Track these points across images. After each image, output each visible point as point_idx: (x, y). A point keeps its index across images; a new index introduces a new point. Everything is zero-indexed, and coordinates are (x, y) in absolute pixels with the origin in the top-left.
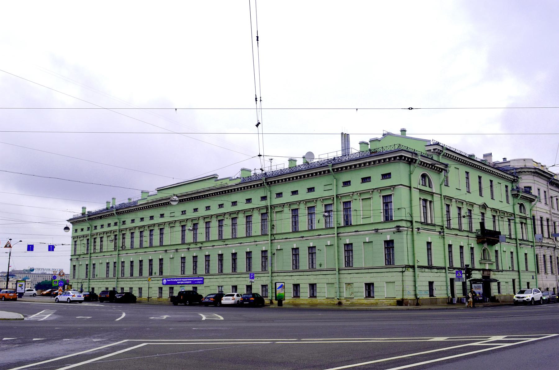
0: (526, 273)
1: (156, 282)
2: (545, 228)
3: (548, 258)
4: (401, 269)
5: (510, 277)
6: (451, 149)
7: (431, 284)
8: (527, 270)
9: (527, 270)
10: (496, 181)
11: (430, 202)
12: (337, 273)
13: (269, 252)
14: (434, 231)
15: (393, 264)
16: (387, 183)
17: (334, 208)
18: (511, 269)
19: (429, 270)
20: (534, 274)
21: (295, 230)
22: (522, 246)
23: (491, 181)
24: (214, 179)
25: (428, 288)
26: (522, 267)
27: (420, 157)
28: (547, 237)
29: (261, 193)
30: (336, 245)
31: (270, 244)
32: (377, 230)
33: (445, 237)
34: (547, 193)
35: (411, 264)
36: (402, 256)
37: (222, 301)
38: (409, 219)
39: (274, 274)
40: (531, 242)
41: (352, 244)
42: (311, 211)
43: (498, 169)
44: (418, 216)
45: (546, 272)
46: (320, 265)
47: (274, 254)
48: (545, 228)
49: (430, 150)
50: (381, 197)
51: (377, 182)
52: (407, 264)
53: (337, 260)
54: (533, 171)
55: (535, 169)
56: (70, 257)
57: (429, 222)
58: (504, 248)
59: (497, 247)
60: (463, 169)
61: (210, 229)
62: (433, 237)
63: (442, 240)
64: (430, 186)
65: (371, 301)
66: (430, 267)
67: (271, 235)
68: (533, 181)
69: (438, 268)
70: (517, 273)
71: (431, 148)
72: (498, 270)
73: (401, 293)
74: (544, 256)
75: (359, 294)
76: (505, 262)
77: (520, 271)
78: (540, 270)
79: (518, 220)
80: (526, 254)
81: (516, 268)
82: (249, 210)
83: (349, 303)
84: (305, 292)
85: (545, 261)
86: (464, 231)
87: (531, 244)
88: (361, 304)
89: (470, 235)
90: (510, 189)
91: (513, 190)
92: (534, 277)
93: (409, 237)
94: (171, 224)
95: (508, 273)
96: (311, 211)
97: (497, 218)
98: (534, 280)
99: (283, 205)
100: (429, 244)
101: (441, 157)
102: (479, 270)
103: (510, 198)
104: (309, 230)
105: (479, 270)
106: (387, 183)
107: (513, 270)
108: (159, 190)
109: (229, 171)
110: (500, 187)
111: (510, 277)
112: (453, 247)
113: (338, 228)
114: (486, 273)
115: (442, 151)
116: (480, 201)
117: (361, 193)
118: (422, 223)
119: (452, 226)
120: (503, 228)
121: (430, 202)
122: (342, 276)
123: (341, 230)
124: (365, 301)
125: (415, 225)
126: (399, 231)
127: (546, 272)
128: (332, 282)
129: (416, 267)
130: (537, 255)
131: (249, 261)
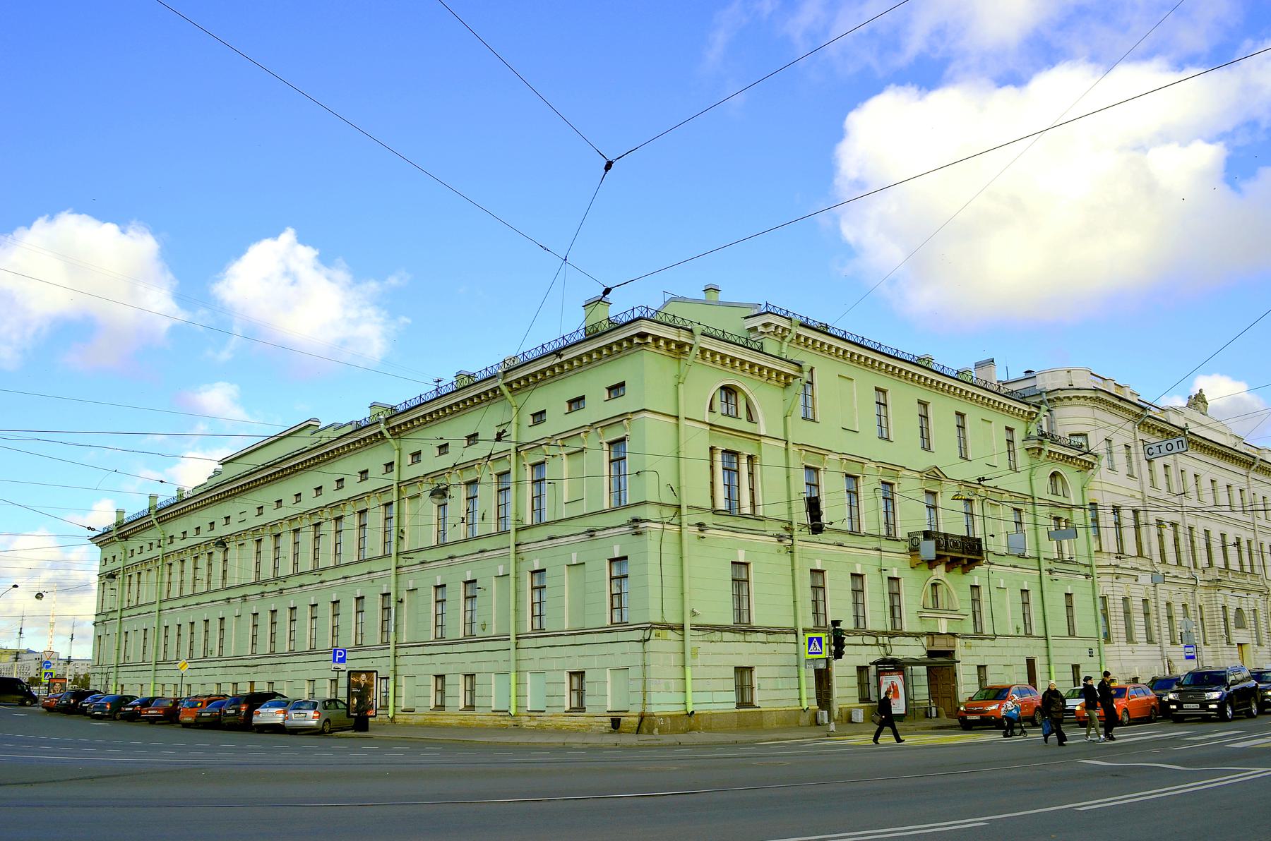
0: (1071, 642)
2: (1129, 534)
3: (1136, 604)
4: (639, 635)
5: (1018, 652)
6: (865, 343)
7: (743, 672)
8: (1071, 633)
9: (1071, 633)
10: (974, 415)
11: (750, 457)
12: (513, 647)
13: (393, 596)
14: (762, 533)
16: (618, 406)
18: (1022, 633)
19: (739, 637)
20: (1094, 645)
22: (1055, 576)
23: (961, 415)
25: (855, 681)
26: (1058, 624)
27: (698, 338)
28: (1237, 568)
30: (512, 574)
31: (393, 578)
33: (796, 548)
34: (1132, 450)
35: (673, 619)
36: (649, 602)
37: (255, 718)
38: (669, 498)
39: (401, 652)
40: (1086, 566)
43: (1009, 395)
44: (696, 493)
45: (1130, 639)
47: (401, 601)
48: (1129, 534)
49: (754, 329)
50: (606, 447)
51: (599, 407)
52: (659, 620)
53: (512, 613)
54: (1089, 394)
55: (1096, 390)
56: (93, 618)
57: (1066, 557)
58: (999, 580)
59: (977, 575)
60: (866, 381)
62: (759, 550)
63: (787, 559)
64: (750, 419)
65: (580, 719)
66: (743, 628)
67: (398, 554)
68: (1092, 421)
69: (769, 631)
70: (1043, 643)
71: (757, 322)
72: (979, 635)
73: (638, 698)
74: (1125, 599)
76: (1005, 613)
77: (1050, 638)
78: (1113, 635)
79: (1043, 511)
80: (1068, 595)
81: (1037, 629)
83: (535, 723)
84: (456, 699)
85: (1127, 613)
86: (866, 535)
87: (1087, 570)
88: (559, 730)
89: (886, 545)
90: (1019, 435)
91: (1028, 438)
92: (1095, 652)
93: (670, 549)
95: (1012, 641)
97: (977, 509)
98: (1096, 659)
100: (1068, 595)
101: (785, 344)
102: (917, 635)
103: (1022, 459)
105: (917, 635)
106: (618, 406)
107: (1028, 635)
109: (347, 409)
110: (989, 433)
111: (1018, 652)
112: (1074, 597)
113: (517, 530)
114: (940, 645)
115: (790, 331)
116: (924, 461)
118: (1054, 560)
119: (864, 529)
120: (995, 530)
121: (750, 457)
122: (523, 653)
123: (524, 536)
124: (566, 721)
125: (688, 518)
126: (637, 534)
127: (1130, 639)
128: (624, 665)
129: (687, 627)
130: (1104, 599)
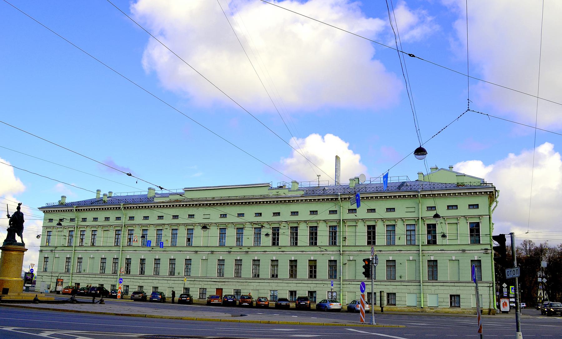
1: (151, 281)
5: (446, 292)
15: (223, 276)
17: (74, 233)
21: (117, 244)
24: (268, 188)
29: (331, 206)
32: (464, 251)
41: (436, 261)
42: (240, 230)
46: (401, 277)
56: (39, 249)
61: (51, 237)
65: (458, 310)
75: (444, 304)
82: (192, 224)
94: (106, 229)
96: (240, 230)
99: (356, 221)
104: (68, 246)
108: (187, 190)
117: (103, 226)
123: (77, 248)
131: (128, 265)
